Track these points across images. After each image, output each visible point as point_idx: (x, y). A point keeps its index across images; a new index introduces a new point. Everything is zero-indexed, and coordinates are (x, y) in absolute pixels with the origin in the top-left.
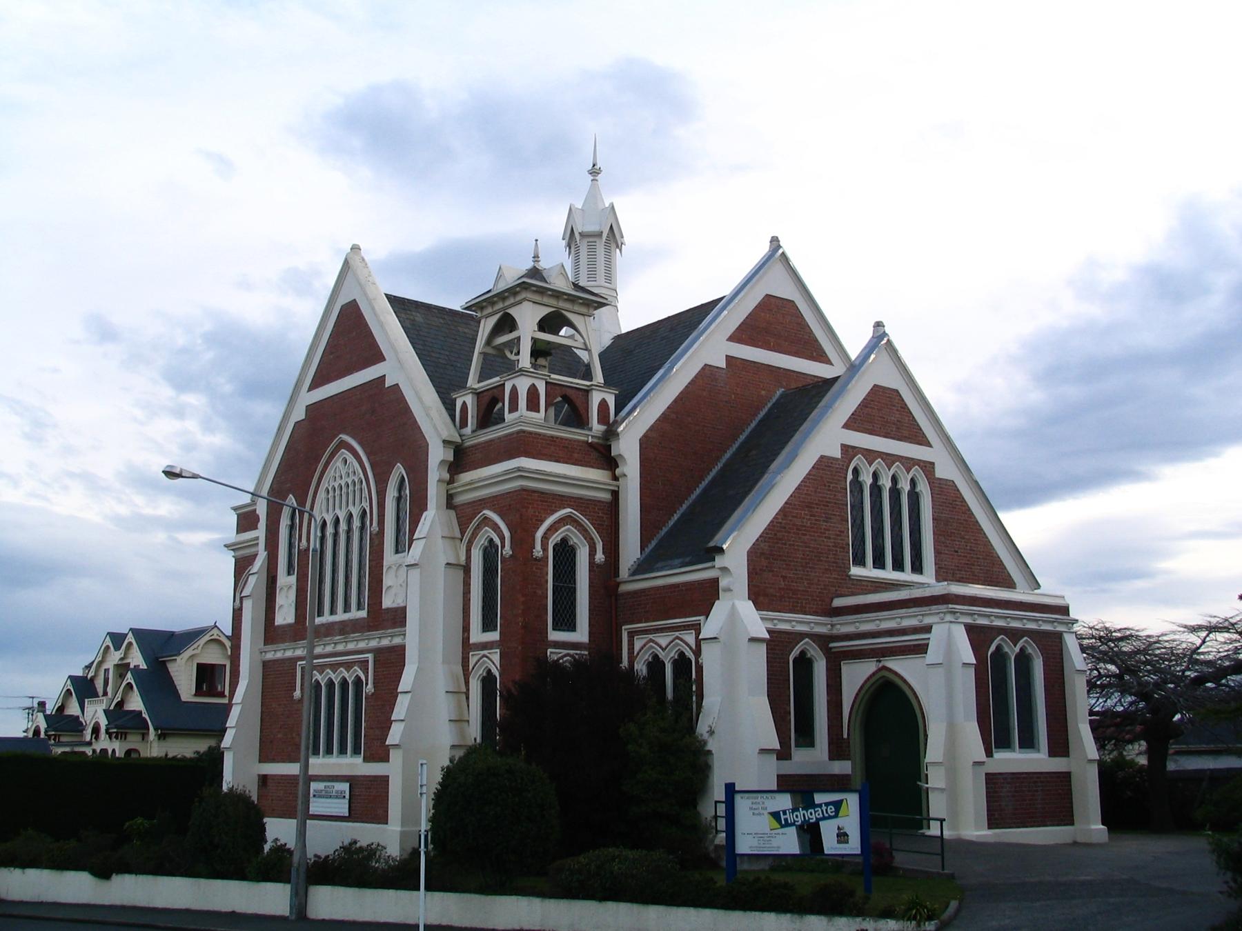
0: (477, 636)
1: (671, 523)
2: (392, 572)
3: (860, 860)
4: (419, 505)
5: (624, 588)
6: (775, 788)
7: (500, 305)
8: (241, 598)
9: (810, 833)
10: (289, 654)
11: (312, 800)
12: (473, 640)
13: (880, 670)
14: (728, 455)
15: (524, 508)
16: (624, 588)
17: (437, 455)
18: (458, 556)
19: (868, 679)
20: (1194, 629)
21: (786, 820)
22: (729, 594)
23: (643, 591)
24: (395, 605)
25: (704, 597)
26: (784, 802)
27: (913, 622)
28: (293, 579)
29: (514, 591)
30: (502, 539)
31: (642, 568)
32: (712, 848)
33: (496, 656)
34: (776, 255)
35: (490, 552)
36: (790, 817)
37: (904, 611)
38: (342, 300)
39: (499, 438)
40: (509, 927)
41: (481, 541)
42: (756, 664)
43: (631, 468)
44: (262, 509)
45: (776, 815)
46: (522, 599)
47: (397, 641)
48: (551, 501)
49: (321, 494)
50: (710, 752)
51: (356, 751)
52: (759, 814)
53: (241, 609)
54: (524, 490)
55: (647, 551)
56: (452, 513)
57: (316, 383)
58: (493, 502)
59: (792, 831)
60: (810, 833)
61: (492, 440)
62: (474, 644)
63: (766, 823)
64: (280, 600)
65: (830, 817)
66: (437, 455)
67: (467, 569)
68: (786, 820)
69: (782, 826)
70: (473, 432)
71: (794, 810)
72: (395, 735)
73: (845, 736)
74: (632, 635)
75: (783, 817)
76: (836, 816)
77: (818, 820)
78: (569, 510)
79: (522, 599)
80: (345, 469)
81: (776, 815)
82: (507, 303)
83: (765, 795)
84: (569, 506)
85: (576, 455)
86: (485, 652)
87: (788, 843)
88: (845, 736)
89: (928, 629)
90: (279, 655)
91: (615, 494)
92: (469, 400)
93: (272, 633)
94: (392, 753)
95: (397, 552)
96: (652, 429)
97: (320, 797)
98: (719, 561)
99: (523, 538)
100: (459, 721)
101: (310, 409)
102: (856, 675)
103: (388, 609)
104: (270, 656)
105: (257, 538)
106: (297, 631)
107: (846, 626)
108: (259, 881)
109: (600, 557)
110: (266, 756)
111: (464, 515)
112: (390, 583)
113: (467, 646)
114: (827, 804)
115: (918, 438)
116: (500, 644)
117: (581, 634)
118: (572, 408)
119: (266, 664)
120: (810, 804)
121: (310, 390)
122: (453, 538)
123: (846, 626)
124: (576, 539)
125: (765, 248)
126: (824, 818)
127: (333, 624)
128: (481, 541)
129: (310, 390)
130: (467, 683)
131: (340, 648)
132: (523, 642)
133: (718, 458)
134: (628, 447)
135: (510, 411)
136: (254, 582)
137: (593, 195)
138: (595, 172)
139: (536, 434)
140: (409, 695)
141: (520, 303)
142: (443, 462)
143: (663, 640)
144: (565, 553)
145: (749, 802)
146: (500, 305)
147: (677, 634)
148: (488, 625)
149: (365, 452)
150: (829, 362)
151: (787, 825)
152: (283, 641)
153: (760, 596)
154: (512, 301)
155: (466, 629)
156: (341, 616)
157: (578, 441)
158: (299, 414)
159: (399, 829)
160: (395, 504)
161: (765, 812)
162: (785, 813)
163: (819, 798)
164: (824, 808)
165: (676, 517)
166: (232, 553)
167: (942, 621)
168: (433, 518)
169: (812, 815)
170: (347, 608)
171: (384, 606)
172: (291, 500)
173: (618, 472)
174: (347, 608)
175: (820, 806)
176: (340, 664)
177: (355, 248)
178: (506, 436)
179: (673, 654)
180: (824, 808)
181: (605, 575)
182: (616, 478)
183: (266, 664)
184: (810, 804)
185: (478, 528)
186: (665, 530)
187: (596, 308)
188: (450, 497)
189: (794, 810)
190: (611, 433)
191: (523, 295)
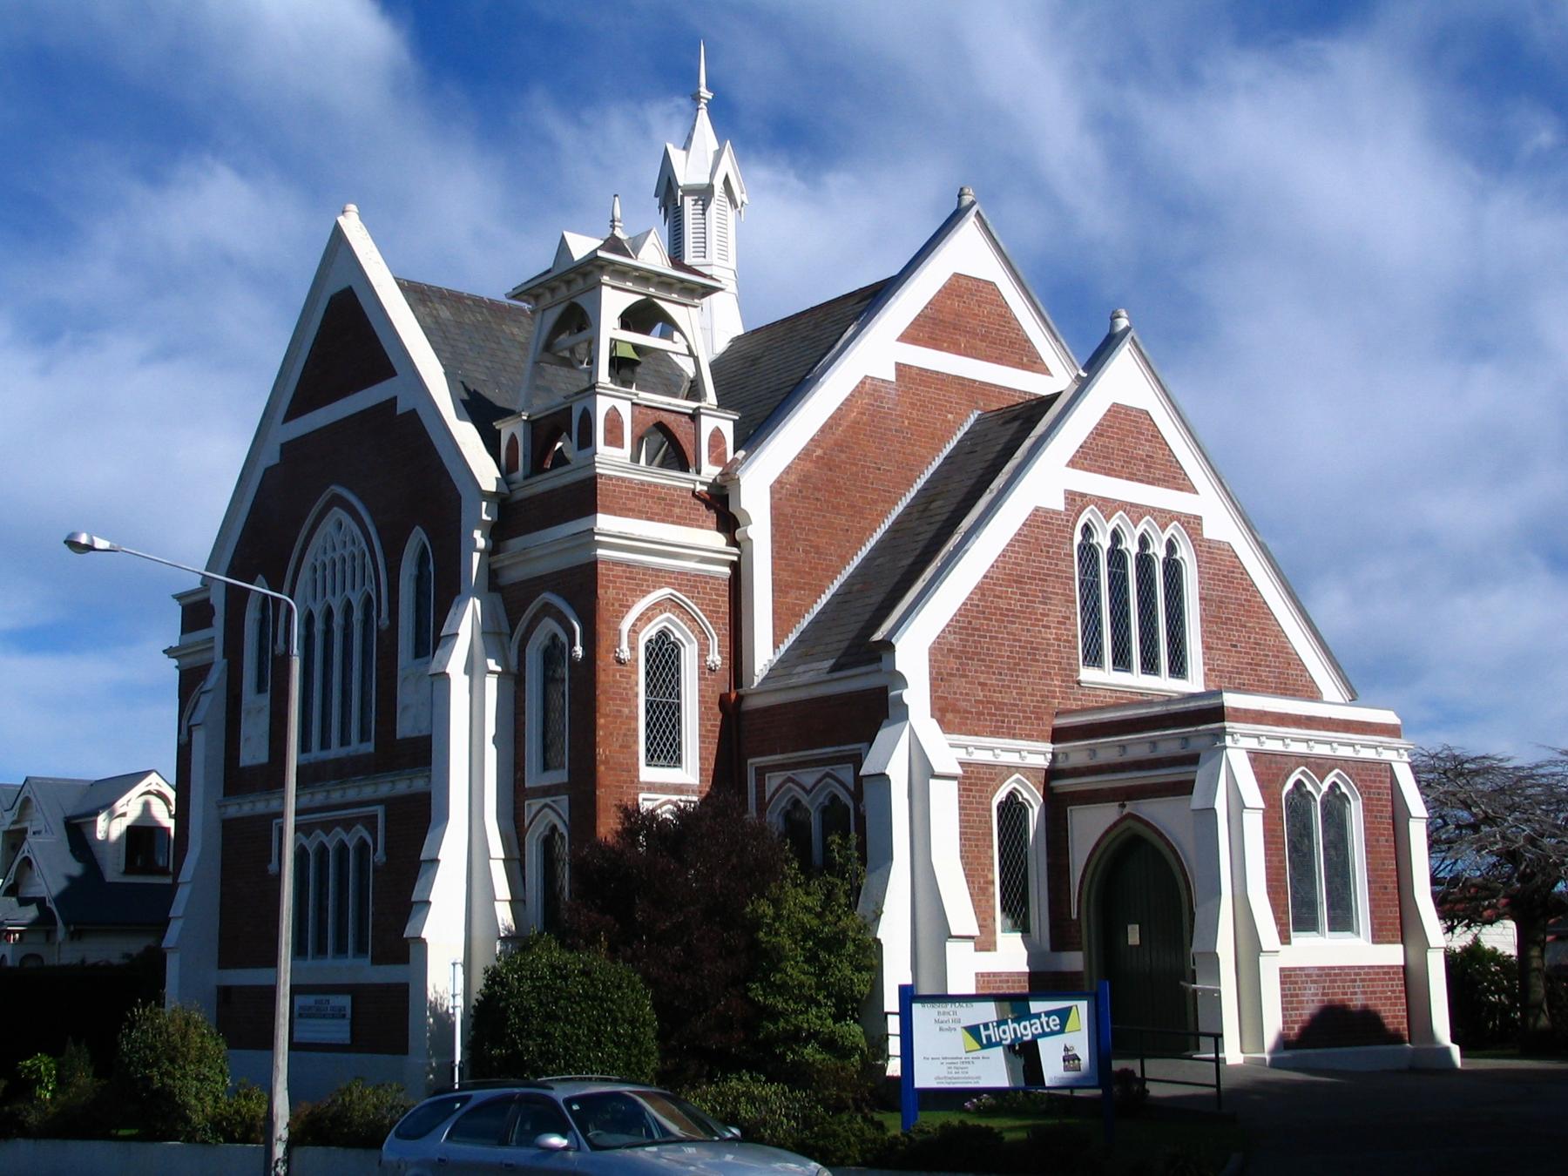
0: (534, 777)
38: (333, 287)
45: (973, 1031)
47: (419, 784)
51: (361, 949)
52: (949, 1029)
57: (293, 413)
59: (999, 1052)
63: (960, 1042)
65: (1053, 1033)
68: (989, 1037)
69: (983, 1047)
70: (526, 478)
71: (1000, 1023)
73: (1074, 916)
75: (983, 1033)
76: (1062, 1031)
81: (973, 1031)
84: (668, 584)
87: (993, 1072)
88: (1074, 916)
105: (212, 639)
109: (715, 658)
124: (681, 633)
126: (1044, 1034)
144: (664, 655)
151: (990, 1044)
161: (959, 1027)
162: (986, 1026)
164: (1044, 1019)
166: (175, 662)
169: (1027, 1031)
171: (398, 737)
175: (1038, 1016)
176: (357, 820)
180: (1044, 1019)
182: (733, 542)
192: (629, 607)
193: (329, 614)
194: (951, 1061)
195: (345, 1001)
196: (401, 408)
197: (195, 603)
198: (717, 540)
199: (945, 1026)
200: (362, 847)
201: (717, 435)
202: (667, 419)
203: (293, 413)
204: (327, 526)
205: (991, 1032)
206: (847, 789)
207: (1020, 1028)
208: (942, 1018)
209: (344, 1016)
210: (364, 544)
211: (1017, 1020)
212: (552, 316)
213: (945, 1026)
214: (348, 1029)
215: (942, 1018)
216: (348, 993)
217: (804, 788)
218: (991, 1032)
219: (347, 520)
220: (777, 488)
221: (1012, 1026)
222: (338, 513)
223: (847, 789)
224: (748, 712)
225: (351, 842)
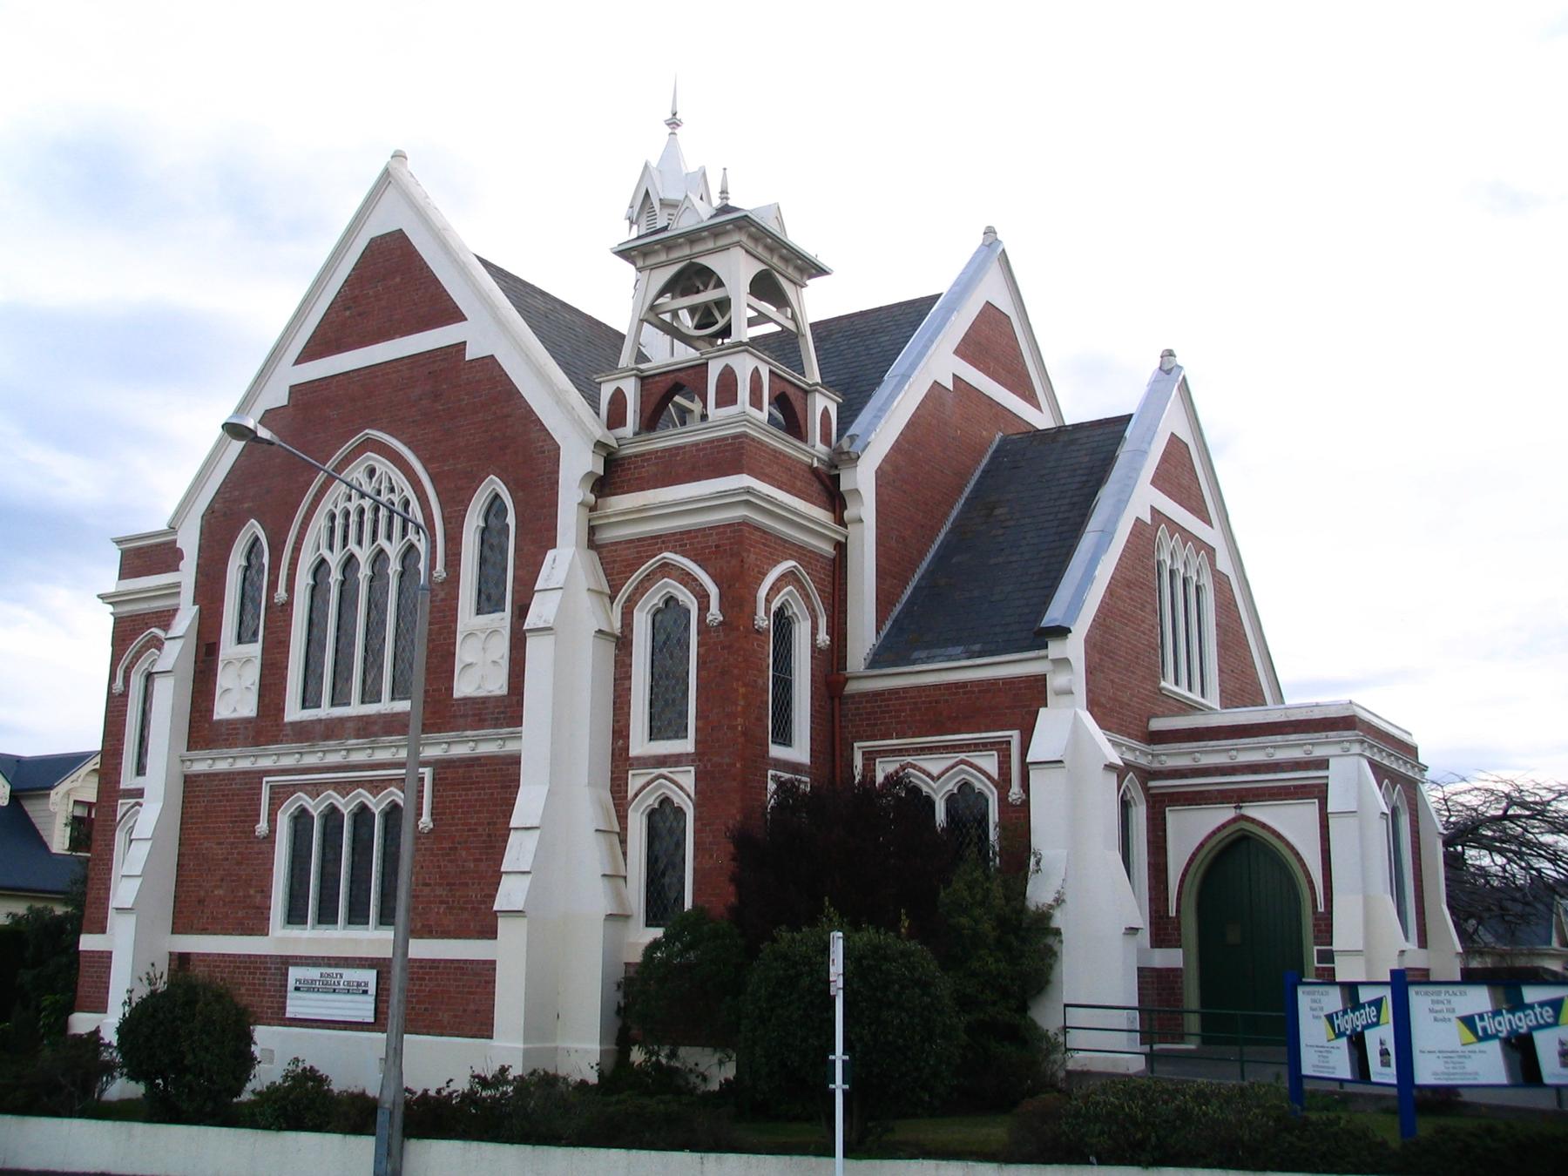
0: (640, 744)
1: (905, 598)
2: (230, 669)
3: (1394, 1091)
4: (539, 534)
5: (852, 687)
6: (1459, 978)
7: (686, 251)
8: (149, 677)
9: (1521, 1050)
10: (244, 764)
11: (291, 994)
12: (633, 752)
13: (1234, 820)
14: (954, 513)
15: (732, 552)
16: (852, 687)
17: (577, 464)
18: (610, 623)
19: (1214, 833)
20: (1550, 790)
21: (1484, 1029)
22: (1066, 699)
23: (894, 692)
24: (482, 693)
25: (1024, 702)
26: (1478, 999)
27: (1297, 754)
28: (255, 649)
29: (716, 676)
30: (703, 597)
31: (880, 658)
32: (1062, 1074)
33: (687, 778)
34: (992, 251)
35: (669, 617)
36: (1490, 1025)
37: (1279, 738)
38: (378, 226)
39: (696, 444)
40: (92, 1170)
41: (654, 598)
42: (1104, 797)
43: (865, 509)
44: (189, 542)
45: (1468, 1021)
46: (742, 690)
47: (511, 747)
48: (779, 547)
49: (320, 522)
50: (1057, 932)
51: (386, 918)
52: (1444, 1020)
53: (125, 695)
54: (744, 524)
55: (882, 634)
56: (594, 555)
57: (312, 352)
58: (683, 541)
59: (1494, 1047)
60: (1521, 1050)
61: (678, 448)
62: (637, 758)
63: (1455, 1035)
64: (224, 679)
65: (1547, 1026)
66: (577, 464)
67: (623, 643)
68: (1484, 1029)
69: (1480, 1039)
70: (636, 434)
71: (1496, 1013)
72: (511, 893)
73: (1172, 913)
74: (870, 757)
75: (1479, 1025)
76: (1556, 1023)
77: (1531, 1029)
78: (793, 563)
79: (742, 690)
80: (377, 476)
81: (1468, 1021)
82: (698, 248)
83: (1443, 989)
84: (792, 557)
85: (799, 484)
86: (664, 771)
87: (1487, 1066)
88: (1172, 913)
89: (1323, 764)
90: (222, 766)
91: (841, 547)
92: (630, 388)
93: (203, 729)
94: (502, 924)
95: (240, 640)
96: (887, 459)
97: (308, 990)
98: (1055, 649)
99: (737, 597)
100: (616, 878)
101: (294, 389)
102: (1190, 830)
103: (466, 700)
104: (201, 767)
105: (178, 585)
106: (267, 725)
107: (1175, 757)
108: (280, 1129)
109: (823, 638)
110: (182, 923)
111: (618, 563)
112: (226, 686)
113: (621, 761)
114: (1542, 1004)
115: (1201, 513)
116: (699, 758)
117: (799, 750)
118: (789, 412)
119: (190, 781)
120: (1517, 1005)
121: (297, 362)
122: (601, 593)
123: (1175, 757)
124: (797, 609)
125: (977, 240)
126: (1540, 1027)
127: (342, 720)
128: (654, 598)
129: (297, 362)
130: (622, 818)
131: (359, 757)
132: (728, 759)
133: (946, 515)
134: (862, 480)
135: (718, 405)
136: (175, 652)
137: (671, 152)
138: (674, 123)
139: (760, 442)
140: (538, 832)
141: (726, 248)
142: (590, 474)
143: (934, 765)
144: (783, 623)
145: (1429, 999)
146: (686, 251)
147: (962, 756)
148: (664, 723)
149: (419, 457)
150: (1038, 407)
151: (1486, 1037)
152: (230, 745)
153: (1104, 708)
154: (710, 245)
155: (621, 732)
156: (356, 709)
157: (800, 462)
158: (277, 396)
159: (521, 1046)
160: (240, 577)
161: (1452, 1016)
162: (1481, 1017)
163: (1531, 994)
164: (1538, 1010)
165: (908, 591)
166: (110, 608)
167: (1346, 753)
168: (566, 564)
169: (1522, 1022)
170: (371, 695)
171: (456, 694)
172: (254, 528)
173: (847, 514)
174: (339, 698)
175: (1531, 1007)
176: (388, 782)
177: (399, 156)
178: (711, 441)
179: (952, 786)
180: (1538, 1010)
181: (831, 662)
182: (841, 521)
183: (190, 781)
184: (1517, 1005)
185: (649, 579)
186: (899, 607)
187: (810, 277)
188: (592, 530)
189: (1496, 1013)
190: (842, 458)
191: (736, 237)
192: (765, 575)
193: (350, 563)
194: (1447, 1055)
195: (370, 976)
196: (471, 354)
197: (140, 548)
198: (821, 514)
199: (1439, 1016)
200: (393, 812)
201: (826, 412)
202: (790, 391)
203: (312, 352)
204: (356, 473)
205: (1486, 1023)
206: (989, 777)
207: (1515, 1021)
208: (1438, 1007)
209: (365, 992)
210: (410, 493)
211: (1512, 1011)
212: (664, 275)
213: (1439, 1016)
214: (373, 1006)
215: (1438, 1007)
216: (371, 967)
217: (929, 775)
218: (1486, 1023)
219: (383, 466)
220: (880, 474)
221: (1508, 1016)
222: (372, 459)
223: (989, 777)
224: (852, 696)
225: (377, 805)
